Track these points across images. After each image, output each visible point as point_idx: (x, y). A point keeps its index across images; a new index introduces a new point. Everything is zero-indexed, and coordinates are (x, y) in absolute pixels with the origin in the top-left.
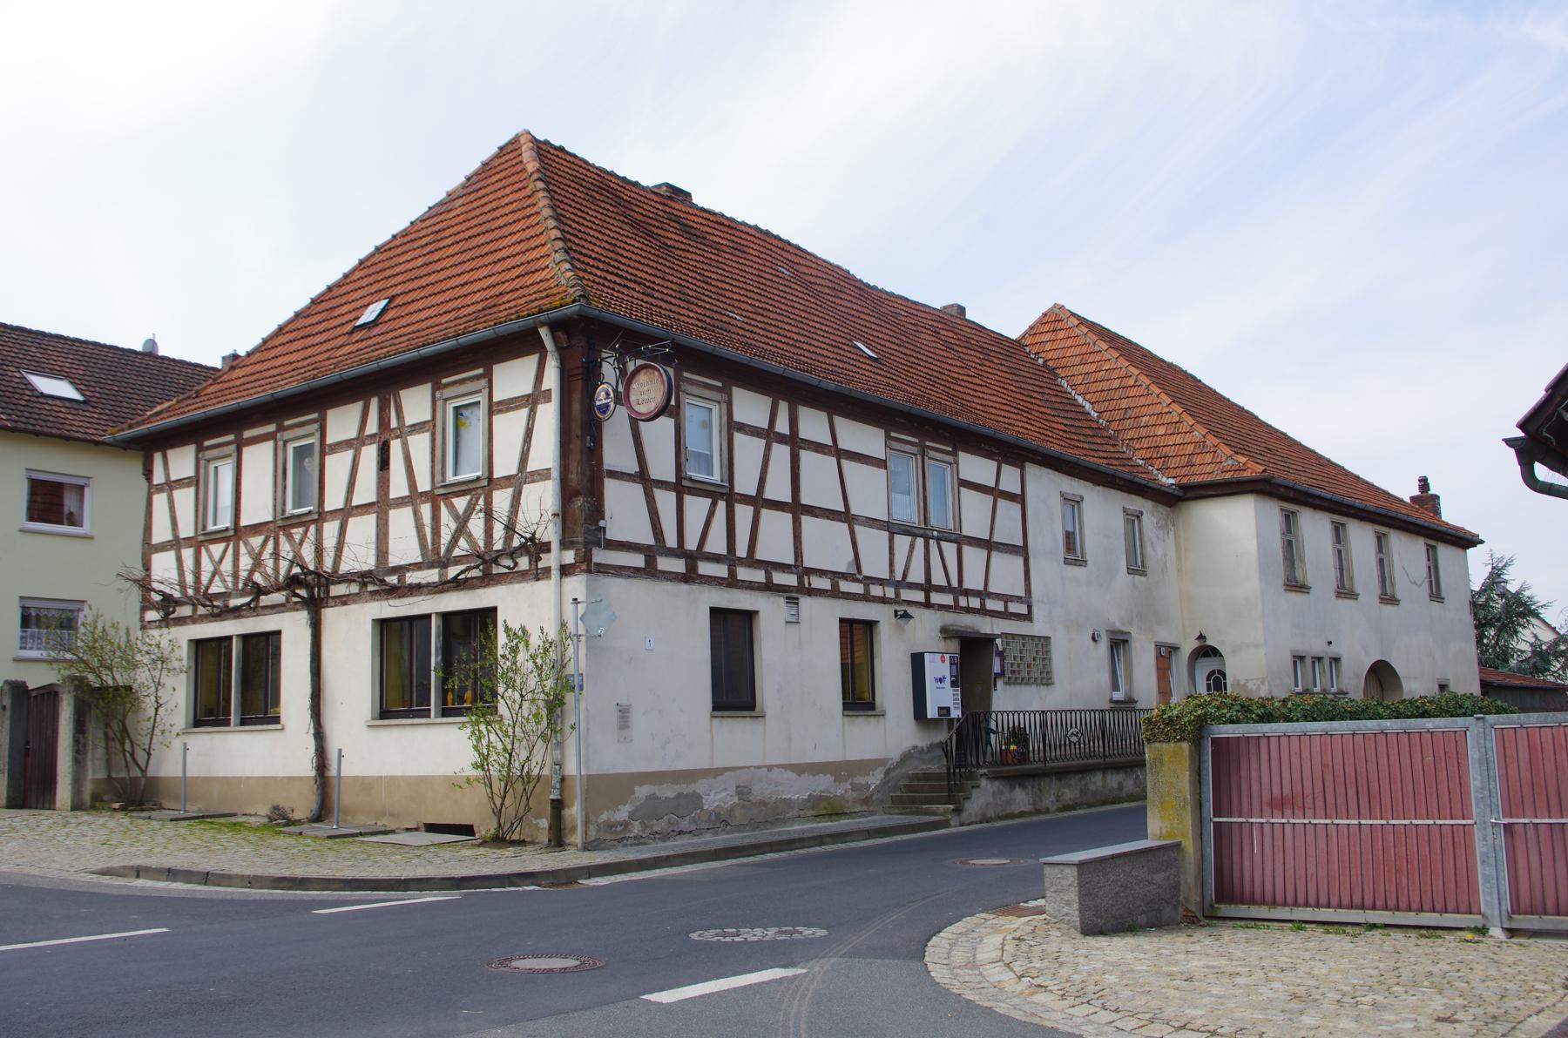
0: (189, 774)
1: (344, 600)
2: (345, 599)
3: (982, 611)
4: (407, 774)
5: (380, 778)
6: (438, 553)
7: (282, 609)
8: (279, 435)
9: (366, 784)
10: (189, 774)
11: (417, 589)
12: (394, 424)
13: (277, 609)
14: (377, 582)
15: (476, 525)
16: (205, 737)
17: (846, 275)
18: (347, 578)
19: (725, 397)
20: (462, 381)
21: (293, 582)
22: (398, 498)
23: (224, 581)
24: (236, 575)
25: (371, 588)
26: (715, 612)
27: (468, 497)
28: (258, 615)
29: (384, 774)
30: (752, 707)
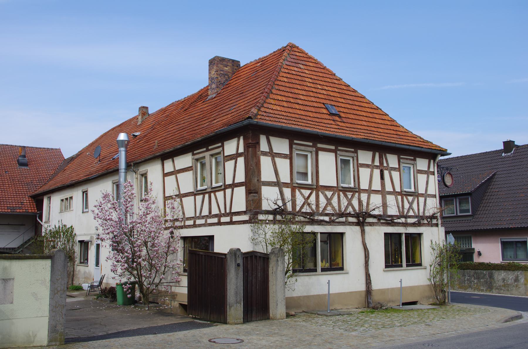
0: (403, 286)
1: (371, 224)
2: (371, 224)
3: (195, 226)
4: (397, 287)
5: (388, 289)
6: (404, 213)
7: (343, 224)
8: (314, 149)
9: (383, 292)
10: (403, 286)
11: (398, 224)
12: (385, 165)
13: (341, 224)
14: (389, 221)
15: (415, 206)
16: (307, 278)
17: (439, 149)
18: (374, 216)
19: (356, 155)
20: (407, 159)
21: (357, 215)
22: (389, 191)
23: (310, 207)
24: (317, 205)
25: (382, 221)
26: (386, 234)
27: (412, 197)
28: (331, 225)
29: (389, 287)
30: (342, 269)
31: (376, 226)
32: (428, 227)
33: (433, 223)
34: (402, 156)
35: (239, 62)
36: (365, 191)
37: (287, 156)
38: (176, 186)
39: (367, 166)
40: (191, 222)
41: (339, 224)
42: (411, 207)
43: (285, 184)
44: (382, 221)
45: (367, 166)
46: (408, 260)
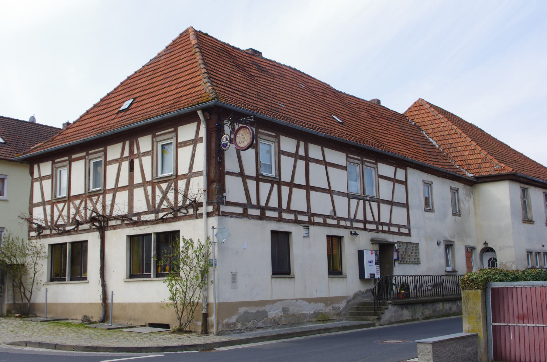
1: (114, 227)
2: (115, 227)
3: (389, 232)
6: (155, 207)
7: (88, 231)
9: (124, 306)
11: (145, 223)
12: (136, 152)
21: (93, 220)
23: (63, 219)
25: (126, 222)
26: (273, 232)
27: (167, 183)
29: (131, 302)
30: (86, 279)
31: (119, 228)
32: (190, 221)
33: (198, 213)
34: (260, 130)
35: (420, 98)
36: (286, 184)
37: (50, 177)
38: (332, 208)
39: (289, 155)
40: (385, 228)
41: (85, 232)
42: (164, 197)
43: (48, 202)
44: (126, 222)
45: (289, 155)
46: (72, 273)
